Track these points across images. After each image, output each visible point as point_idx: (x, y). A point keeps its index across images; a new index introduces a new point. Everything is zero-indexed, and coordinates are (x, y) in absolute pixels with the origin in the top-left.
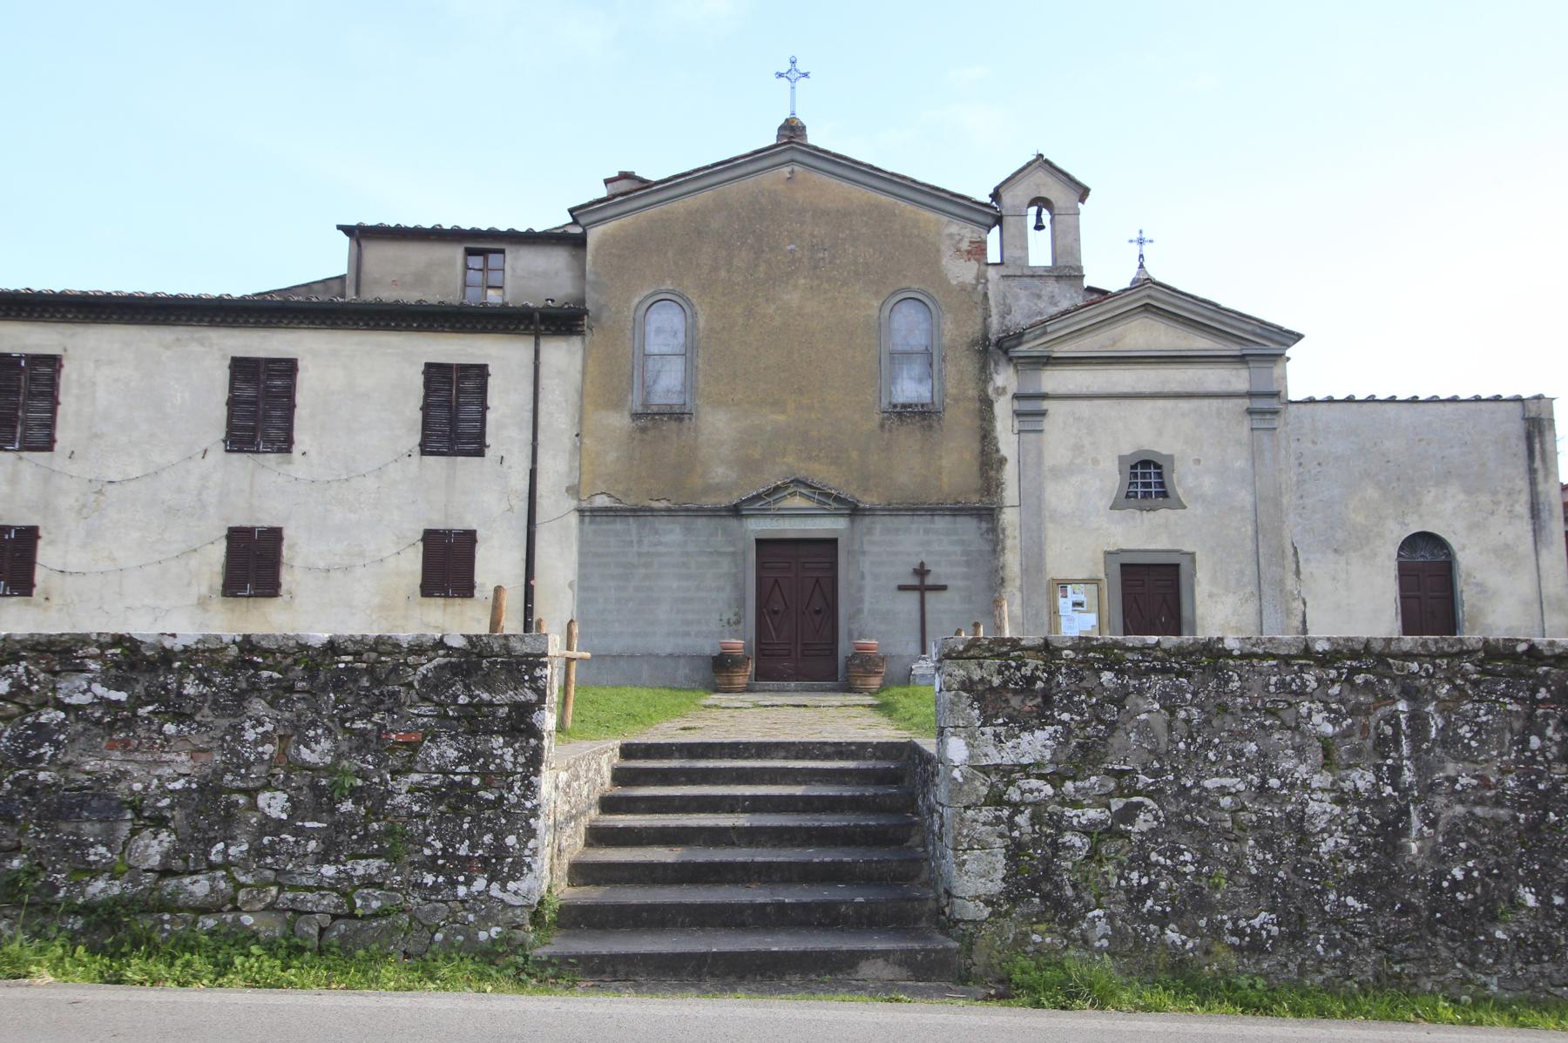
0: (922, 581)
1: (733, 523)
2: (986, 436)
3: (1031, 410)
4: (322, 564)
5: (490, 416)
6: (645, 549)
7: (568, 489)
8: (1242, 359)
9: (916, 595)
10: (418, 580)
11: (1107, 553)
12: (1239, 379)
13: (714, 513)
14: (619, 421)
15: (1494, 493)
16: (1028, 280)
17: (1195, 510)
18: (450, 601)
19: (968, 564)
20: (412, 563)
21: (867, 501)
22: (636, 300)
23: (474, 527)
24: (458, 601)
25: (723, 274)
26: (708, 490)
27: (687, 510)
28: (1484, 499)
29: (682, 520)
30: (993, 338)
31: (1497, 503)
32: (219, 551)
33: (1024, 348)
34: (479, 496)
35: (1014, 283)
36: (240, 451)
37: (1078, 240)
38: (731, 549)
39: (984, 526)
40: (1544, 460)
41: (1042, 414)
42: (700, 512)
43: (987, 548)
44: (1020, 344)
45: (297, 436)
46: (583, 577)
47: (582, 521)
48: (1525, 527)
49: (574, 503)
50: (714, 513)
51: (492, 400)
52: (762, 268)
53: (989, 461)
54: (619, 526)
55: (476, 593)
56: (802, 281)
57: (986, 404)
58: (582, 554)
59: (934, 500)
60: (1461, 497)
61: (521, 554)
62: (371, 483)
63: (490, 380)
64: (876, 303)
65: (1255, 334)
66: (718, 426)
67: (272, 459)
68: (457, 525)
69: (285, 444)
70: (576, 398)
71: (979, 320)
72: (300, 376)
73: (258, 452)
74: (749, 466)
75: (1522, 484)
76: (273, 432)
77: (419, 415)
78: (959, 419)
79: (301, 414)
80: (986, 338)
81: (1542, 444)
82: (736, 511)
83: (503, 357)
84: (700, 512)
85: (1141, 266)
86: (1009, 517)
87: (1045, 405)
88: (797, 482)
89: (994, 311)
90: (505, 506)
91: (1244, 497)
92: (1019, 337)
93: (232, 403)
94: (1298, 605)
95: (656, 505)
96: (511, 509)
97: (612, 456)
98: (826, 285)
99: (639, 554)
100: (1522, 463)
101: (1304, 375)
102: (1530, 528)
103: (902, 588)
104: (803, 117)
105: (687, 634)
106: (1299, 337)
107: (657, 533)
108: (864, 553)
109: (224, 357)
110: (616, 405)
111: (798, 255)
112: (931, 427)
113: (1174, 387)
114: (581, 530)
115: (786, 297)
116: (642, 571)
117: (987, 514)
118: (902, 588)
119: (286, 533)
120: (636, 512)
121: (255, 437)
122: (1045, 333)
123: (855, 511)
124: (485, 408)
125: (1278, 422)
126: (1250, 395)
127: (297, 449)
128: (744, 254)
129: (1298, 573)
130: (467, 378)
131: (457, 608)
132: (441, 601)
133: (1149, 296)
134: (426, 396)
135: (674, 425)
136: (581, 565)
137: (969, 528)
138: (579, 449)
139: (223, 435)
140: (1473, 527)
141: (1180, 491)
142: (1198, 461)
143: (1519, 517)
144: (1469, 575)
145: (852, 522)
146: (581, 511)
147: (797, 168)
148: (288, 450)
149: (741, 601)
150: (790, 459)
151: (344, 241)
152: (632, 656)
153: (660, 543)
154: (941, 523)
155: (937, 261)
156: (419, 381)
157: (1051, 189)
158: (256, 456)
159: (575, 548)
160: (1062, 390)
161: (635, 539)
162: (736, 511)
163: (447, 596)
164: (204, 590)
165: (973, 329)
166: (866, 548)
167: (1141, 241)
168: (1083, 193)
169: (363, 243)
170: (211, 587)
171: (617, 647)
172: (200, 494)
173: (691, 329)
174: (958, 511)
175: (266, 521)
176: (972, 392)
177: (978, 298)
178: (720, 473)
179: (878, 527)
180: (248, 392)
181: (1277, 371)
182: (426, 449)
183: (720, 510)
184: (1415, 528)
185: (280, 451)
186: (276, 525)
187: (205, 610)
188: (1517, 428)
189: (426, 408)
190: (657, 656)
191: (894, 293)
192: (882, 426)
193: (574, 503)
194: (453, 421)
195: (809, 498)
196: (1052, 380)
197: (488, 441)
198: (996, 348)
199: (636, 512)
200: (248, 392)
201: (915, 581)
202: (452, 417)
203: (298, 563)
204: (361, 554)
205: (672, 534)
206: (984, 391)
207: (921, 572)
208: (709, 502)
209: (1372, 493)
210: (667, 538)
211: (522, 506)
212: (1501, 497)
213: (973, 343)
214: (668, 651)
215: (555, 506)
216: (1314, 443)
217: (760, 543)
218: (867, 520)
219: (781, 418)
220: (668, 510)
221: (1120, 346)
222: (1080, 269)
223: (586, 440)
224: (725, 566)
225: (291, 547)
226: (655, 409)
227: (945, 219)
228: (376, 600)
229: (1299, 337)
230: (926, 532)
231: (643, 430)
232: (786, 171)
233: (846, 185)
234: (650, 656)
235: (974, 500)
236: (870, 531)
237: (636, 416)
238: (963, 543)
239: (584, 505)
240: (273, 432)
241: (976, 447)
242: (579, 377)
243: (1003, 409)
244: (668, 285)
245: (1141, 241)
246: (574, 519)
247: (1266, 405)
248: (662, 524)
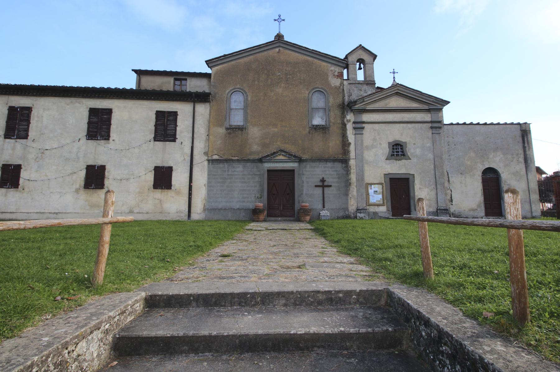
0: (323, 184)
1: (260, 164)
2: (344, 136)
3: (359, 127)
4: (119, 178)
5: (178, 128)
6: (230, 173)
7: (204, 153)
8: (429, 111)
9: (321, 189)
10: (152, 183)
11: (385, 174)
12: (427, 117)
13: (253, 161)
14: (222, 131)
15: (512, 155)
16: (357, 85)
17: (414, 160)
18: (163, 190)
19: (339, 178)
20: (150, 177)
21: (305, 157)
22: (228, 91)
23: (172, 165)
24: (166, 190)
25: (256, 82)
26: (252, 153)
27: (244, 160)
28: (509, 156)
29: (243, 163)
30: (346, 104)
31: (513, 158)
32: (83, 174)
33: (357, 106)
34: (174, 155)
35: (353, 86)
36: (92, 139)
37: (373, 72)
38: (259, 173)
39: (344, 165)
40: (528, 143)
41: (363, 128)
42: (248, 161)
43: (345, 173)
44: (355, 105)
45: (111, 135)
46: (209, 182)
47: (209, 164)
48: (523, 166)
49: (206, 158)
50: (253, 161)
51: (179, 123)
52: (270, 81)
53: (345, 144)
54: (221, 165)
55: (172, 188)
56: (283, 85)
57: (344, 126)
58: (209, 175)
59: (327, 157)
60: (502, 156)
61: (187, 175)
62: (137, 150)
63: (178, 117)
64: (307, 92)
65: (433, 102)
66: (255, 132)
67: (103, 142)
68: (166, 165)
69: (107, 137)
70: (207, 123)
71: (341, 98)
72: (113, 114)
73: (98, 140)
74: (264, 145)
75: (521, 151)
76: (103, 133)
77: (153, 128)
78: (335, 130)
79: (113, 127)
80: (343, 103)
81: (527, 139)
82: (261, 160)
83: (183, 110)
84: (248, 161)
85: (394, 80)
86: (352, 163)
87: (364, 125)
88: (282, 151)
89: (346, 95)
90: (182, 158)
91: (430, 156)
92: (355, 102)
93: (89, 123)
94: (449, 192)
95: (233, 158)
96: (185, 160)
97: (219, 142)
98: (290, 86)
99: (228, 175)
100: (521, 145)
101: (449, 116)
102: (524, 166)
103: (316, 186)
104: (282, 33)
105: (244, 202)
106: (448, 102)
107: (234, 167)
108: (303, 174)
109: (87, 108)
110: (221, 126)
111: (281, 76)
112: (325, 133)
113: (406, 120)
114: (209, 167)
115: (277, 90)
116: (229, 180)
117: (345, 161)
118: (316, 186)
119: (107, 167)
120: (227, 161)
121: (96, 135)
122: (364, 101)
123: (300, 160)
124: (176, 126)
125: (441, 131)
126: (432, 122)
127: (111, 139)
128: (263, 76)
129: (449, 181)
130: (171, 116)
131: (166, 193)
132: (160, 190)
133: (398, 89)
134: (156, 122)
135: (240, 132)
136: (208, 178)
137: (339, 166)
138: (208, 140)
139: (86, 134)
140: (506, 166)
141: (409, 154)
142: (415, 144)
143: (521, 162)
144: (505, 182)
145: (299, 164)
146: (208, 160)
147: (281, 49)
148: (108, 139)
149: (262, 191)
150: (279, 143)
151: (135, 75)
152: (225, 209)
153: (235, 171)
154: (329, 164)
155: (327, 79)
156: (154, 116)
157: (364, 57)
158: (97, 141)
159: (206, 173)
160: (369, 120)
161: (227, 170)
162: (261, 160)
163: (162, 189)
164: (78, 186)
165: (339, 100)
166: (304, 173)
167: (394, 73)
168: (375, 57)
169: (141, 76)
170: (80, 186)
171: (220, 206)
172: (77, 154)
173: (246, 101)
174: (335, 160)
175: (100, 163)
176: (339, 121)
177: (341, 91)
178: (255, 148)
179: (308, 166)
180: (95, 119)
181: (440, 114)
182: (156, 139)
183: (255, 160)
184: (487, 167)
185: (105, 139)
186: (103, 164)
187: (78, 193)
188: (519, 133)
189: (156, 126)
190: (234, 209)
191: (313, 89)
192: (309, 132)
193: (206, 158)
194: (165, 130)
195: (285, 156)
196: (366, 117)
197: (177, 137)
198: (348, 106)
199: (227, 161)
200: (95, 119)
201: (321, 184)
202: (165, 128)
203: (111, 177)
204: (133, 174)
205: (239, 168)
206: (343, 121)
207: (323, 181)
208: (251, 157)
209: (472, 154)
210: (238, 170)
211: (189, 159)
212: (515, 156)
213: (339, 105)
214: (238, 207)
215: (200, 158)
216: (453, 138)
217: (268, 171)
218: (304, 163)
219: (276, 130)
220: (238, 160)
221: (388, 106)
222: (374, 81)
223: (210, 137)
224: (257, 179)
225: (108, 172)
226: (234, 127)
227: (330, 65)
228: (138, 190)
229: (448, 102)
230: (325, 167)
231: (230, 134)
232: (277, 50)
233: (297, 54)
234: (231, 209)
235: (340, 157)
236: (305, 167)
237: (227, 129)
238: (336, 171)
239: (210, 158)
240: (103, 133)
241: (341, 139)
242: (208, 116)
243: (350, 126)
244: (238, 86)
245: (394, 73)
246: (206, 163)
247: (437, 125)
248: (236, 165)
